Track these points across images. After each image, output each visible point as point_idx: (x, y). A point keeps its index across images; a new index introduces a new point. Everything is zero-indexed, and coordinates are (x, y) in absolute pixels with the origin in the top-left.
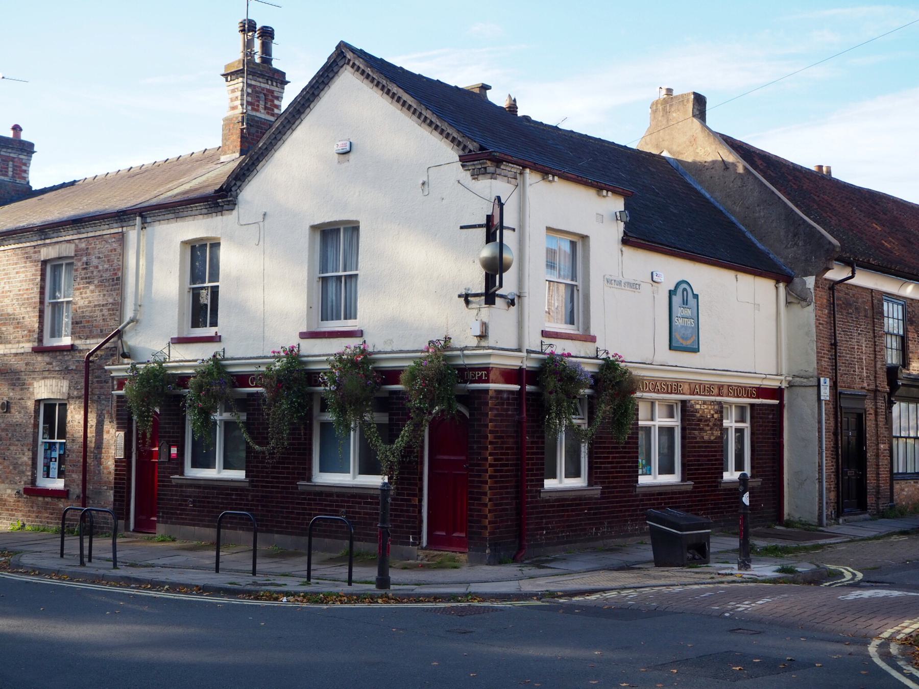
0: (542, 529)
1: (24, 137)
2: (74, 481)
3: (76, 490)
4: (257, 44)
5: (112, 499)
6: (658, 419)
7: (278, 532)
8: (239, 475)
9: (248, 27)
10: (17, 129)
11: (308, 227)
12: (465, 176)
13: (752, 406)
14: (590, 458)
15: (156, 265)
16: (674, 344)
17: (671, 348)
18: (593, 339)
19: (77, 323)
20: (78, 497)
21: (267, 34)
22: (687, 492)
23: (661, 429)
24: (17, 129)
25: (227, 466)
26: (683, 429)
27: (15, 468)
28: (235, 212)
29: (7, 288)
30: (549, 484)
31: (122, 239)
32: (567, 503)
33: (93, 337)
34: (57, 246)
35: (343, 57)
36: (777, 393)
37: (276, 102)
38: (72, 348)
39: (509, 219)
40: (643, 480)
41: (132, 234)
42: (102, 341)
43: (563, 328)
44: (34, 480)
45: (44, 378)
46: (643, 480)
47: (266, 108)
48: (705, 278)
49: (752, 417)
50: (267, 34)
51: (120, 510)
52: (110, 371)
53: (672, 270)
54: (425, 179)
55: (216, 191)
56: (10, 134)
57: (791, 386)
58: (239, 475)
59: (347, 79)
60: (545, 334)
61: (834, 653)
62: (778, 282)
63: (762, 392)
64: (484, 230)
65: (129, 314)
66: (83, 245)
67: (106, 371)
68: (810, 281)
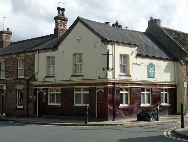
0: (120, 114)
1: (10, 30)
2: (25, 106)
3: (25, 108)
4: (61, 12)
5: (33, 110)
6: (124, 92)
7: (68, 116)
8: (60, 104)
9: (59, 9)
10: (8, 29)
11: (72, 54)
12: (103, 44)
13: (169, 89)
14: (130, 100)
15: (41, 59)
16: (149, 76)
17: (148, 77)
18: (130, 76)
19: (25, 73)
20: (26, 110)
21: (63, 10)
22: (153, 107)
23: (125, 94)
24: (8, 29)
25: (57, 102)
26: (152, 94)
27: (12, 104)
28: (57, 51)
29: (10, 66)
30: (121, 105)
31: (34, 56)
32: (124, 109)
33: (29, 76)
34: (20, 57)
35: (79, 20)
36: (175, 86)
37: (66, 25)
38: (24, 79)
39: (110, 53)
40: (142, 105)
41: (36, 55)
42: (30, 77)
43: (122, 74)
44: (16, 107)
45: (18, 85)
46: (142, 105)
47: (63, 26)
48: (155, 62)
49: (169, 91)
50: (63, 10)
51: (35, 112)
52: (32, 84)
53: (148, 61)
54: (95, 45)
55: (54, 47)
56: (6, 30)
57: (178, 84)
58: (60, 104)
59: (79, 24)
60: (119, 75)
61: (138, 124)
62: (175, 61)
63: (171, 86)
64: (106, 55)
65: (36, 72)
66: (26, 57)
67: (31, 83)
68: (182, 61)
